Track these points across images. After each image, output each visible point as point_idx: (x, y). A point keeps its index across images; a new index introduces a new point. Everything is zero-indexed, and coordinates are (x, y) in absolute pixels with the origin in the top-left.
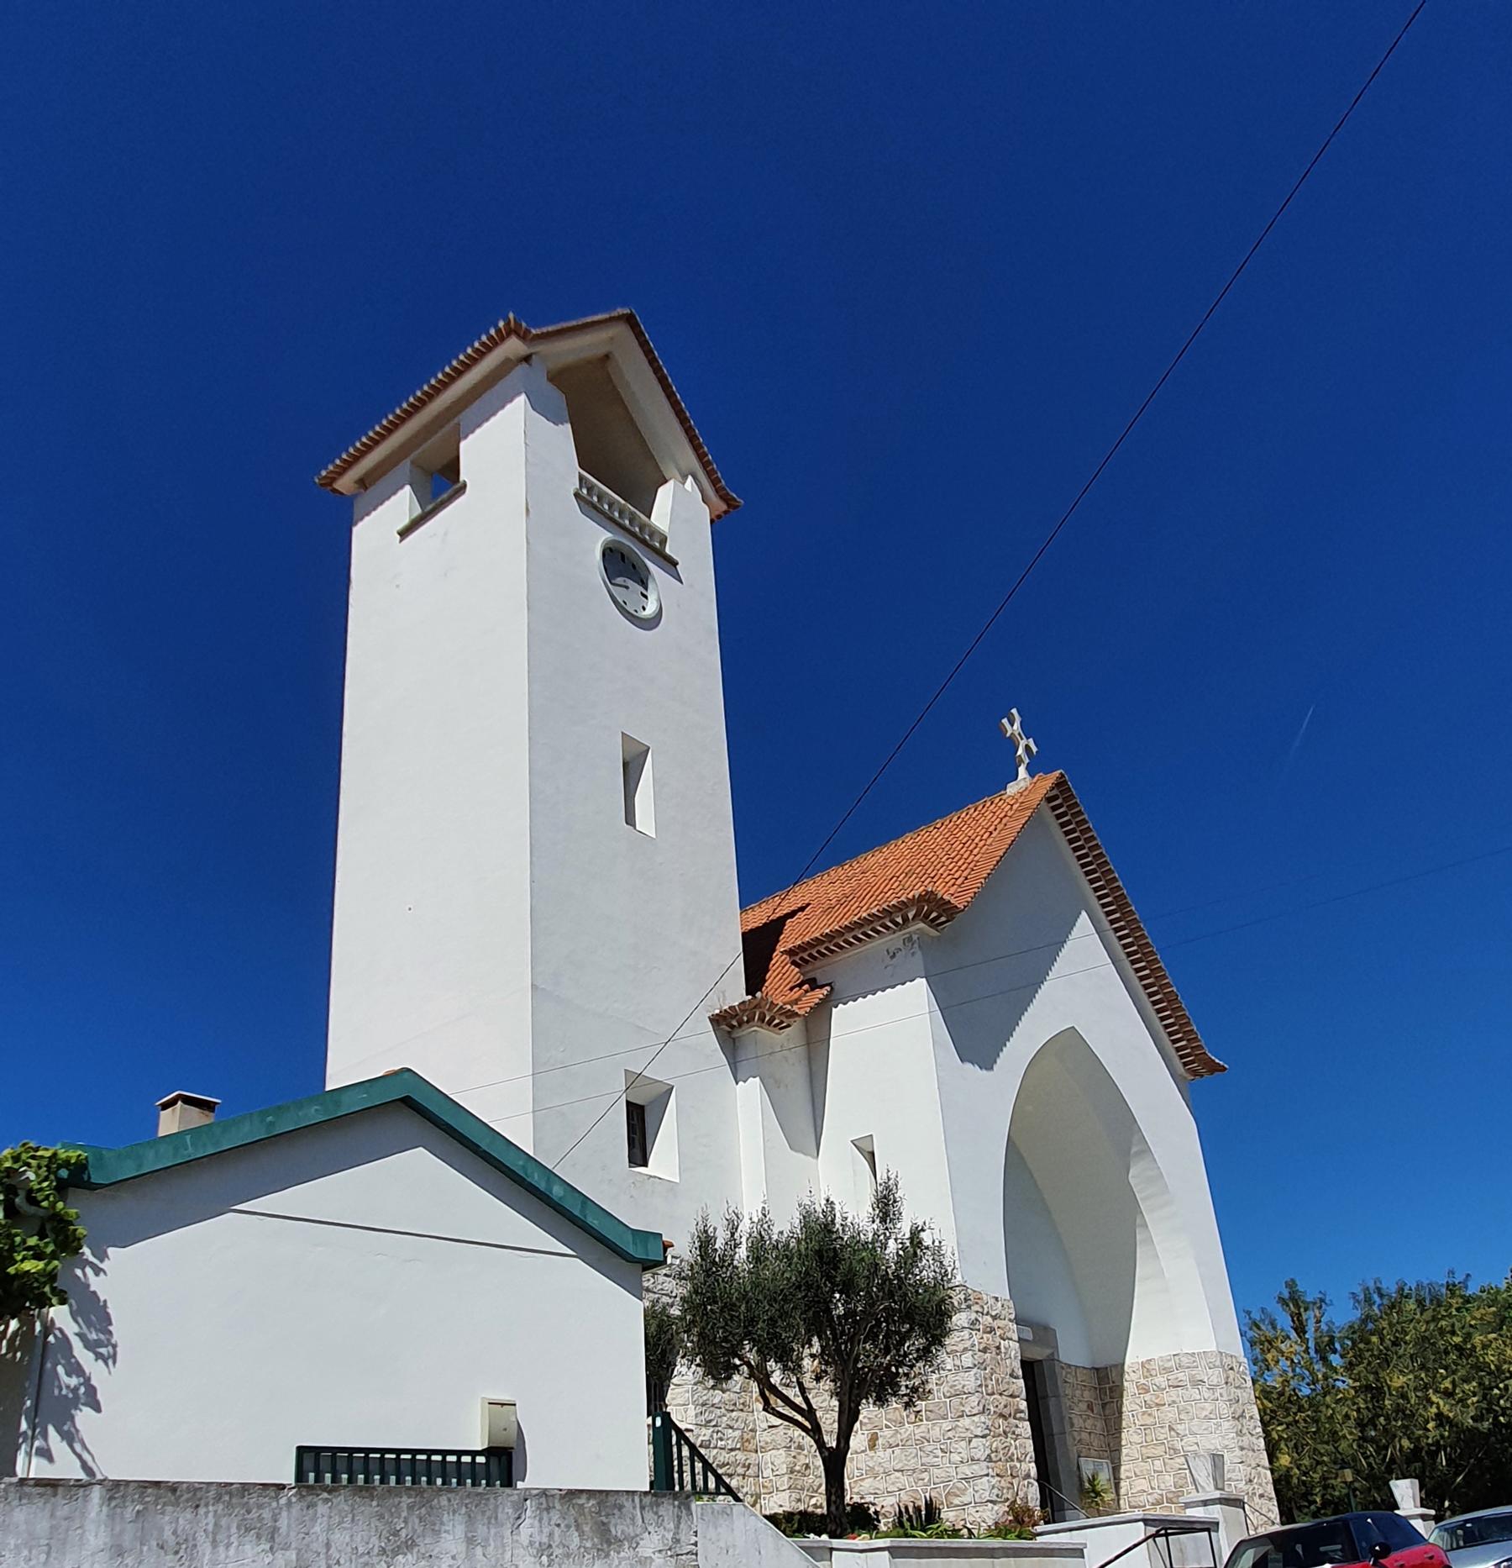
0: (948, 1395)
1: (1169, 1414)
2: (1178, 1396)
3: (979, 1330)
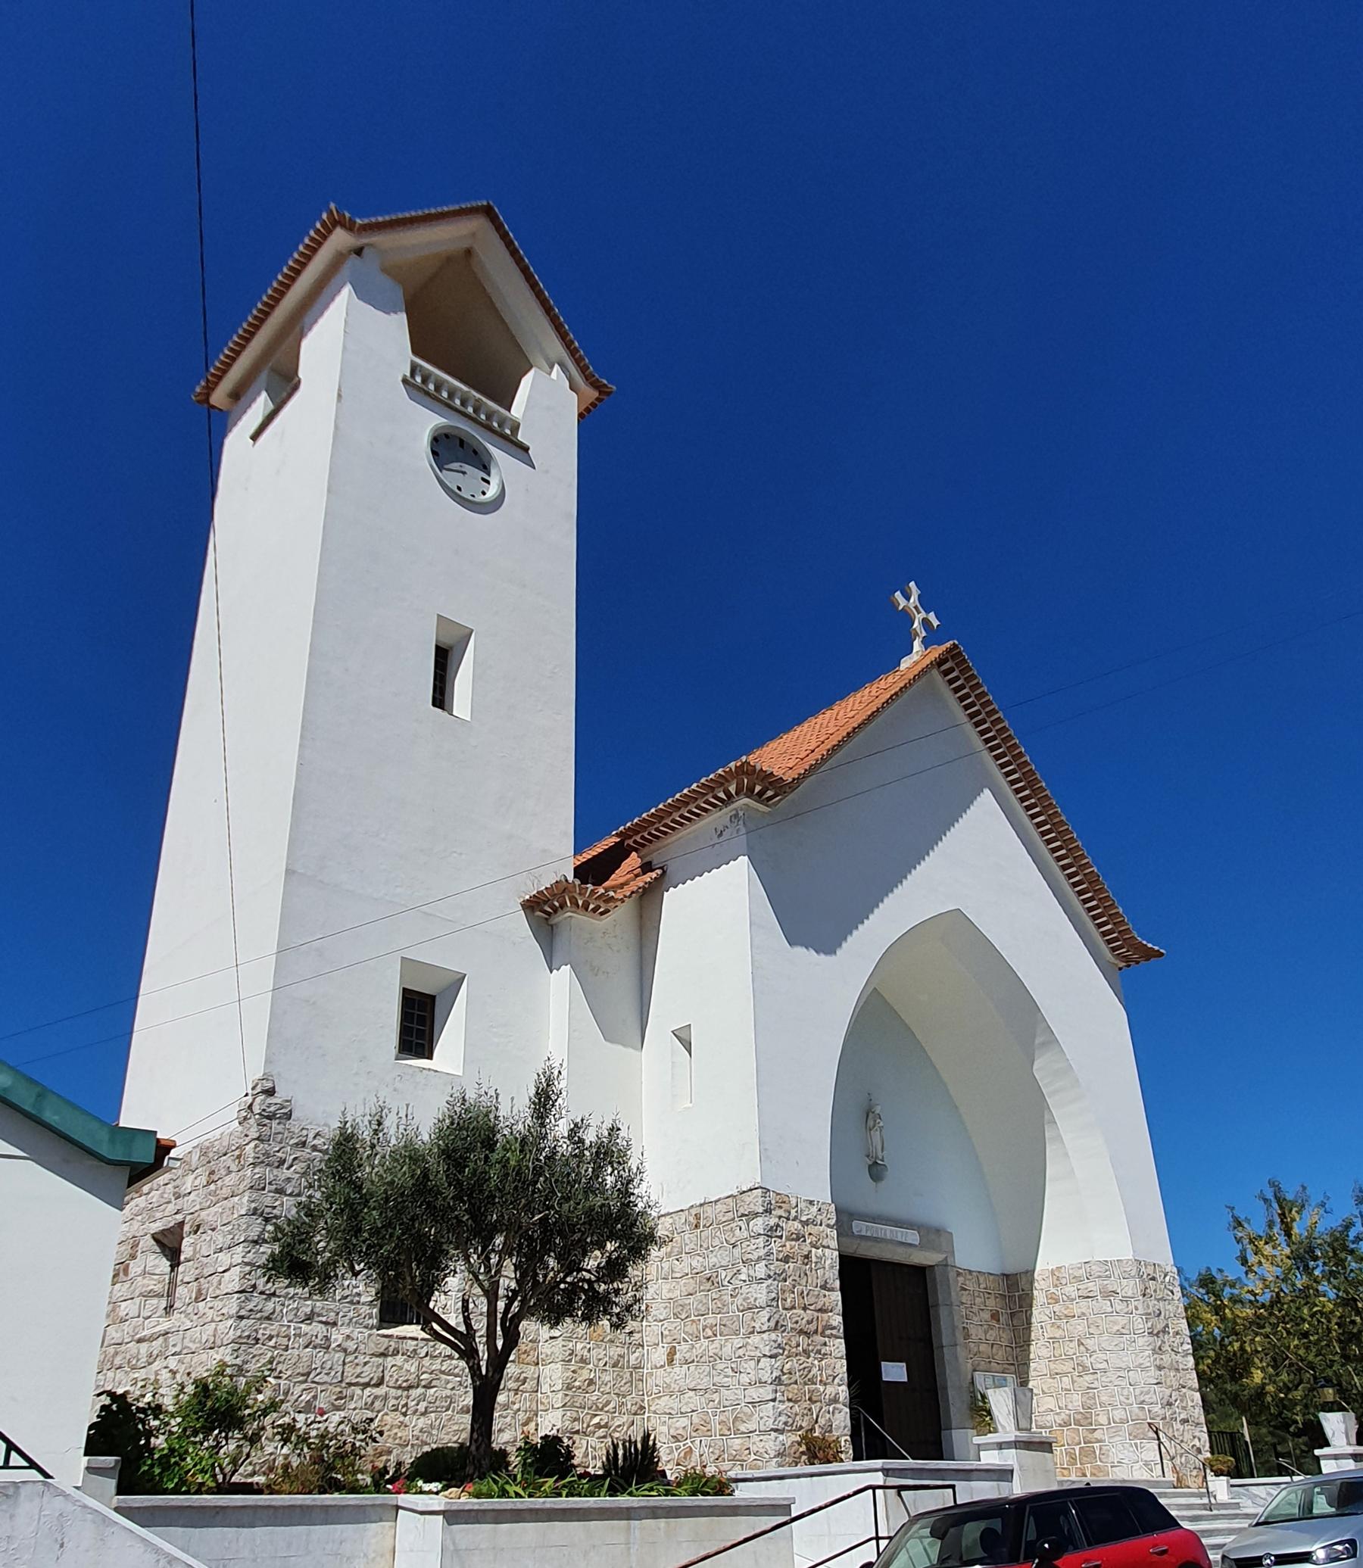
0: (741, 1308)
1: (1079, 1327)
2: (1089, 1308)
3: (781, 1237)
